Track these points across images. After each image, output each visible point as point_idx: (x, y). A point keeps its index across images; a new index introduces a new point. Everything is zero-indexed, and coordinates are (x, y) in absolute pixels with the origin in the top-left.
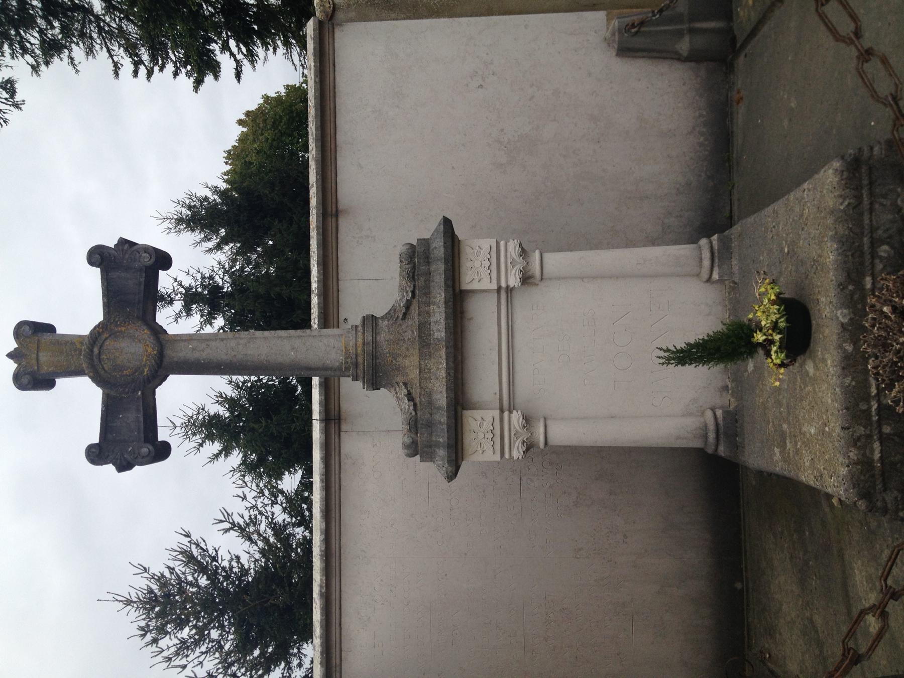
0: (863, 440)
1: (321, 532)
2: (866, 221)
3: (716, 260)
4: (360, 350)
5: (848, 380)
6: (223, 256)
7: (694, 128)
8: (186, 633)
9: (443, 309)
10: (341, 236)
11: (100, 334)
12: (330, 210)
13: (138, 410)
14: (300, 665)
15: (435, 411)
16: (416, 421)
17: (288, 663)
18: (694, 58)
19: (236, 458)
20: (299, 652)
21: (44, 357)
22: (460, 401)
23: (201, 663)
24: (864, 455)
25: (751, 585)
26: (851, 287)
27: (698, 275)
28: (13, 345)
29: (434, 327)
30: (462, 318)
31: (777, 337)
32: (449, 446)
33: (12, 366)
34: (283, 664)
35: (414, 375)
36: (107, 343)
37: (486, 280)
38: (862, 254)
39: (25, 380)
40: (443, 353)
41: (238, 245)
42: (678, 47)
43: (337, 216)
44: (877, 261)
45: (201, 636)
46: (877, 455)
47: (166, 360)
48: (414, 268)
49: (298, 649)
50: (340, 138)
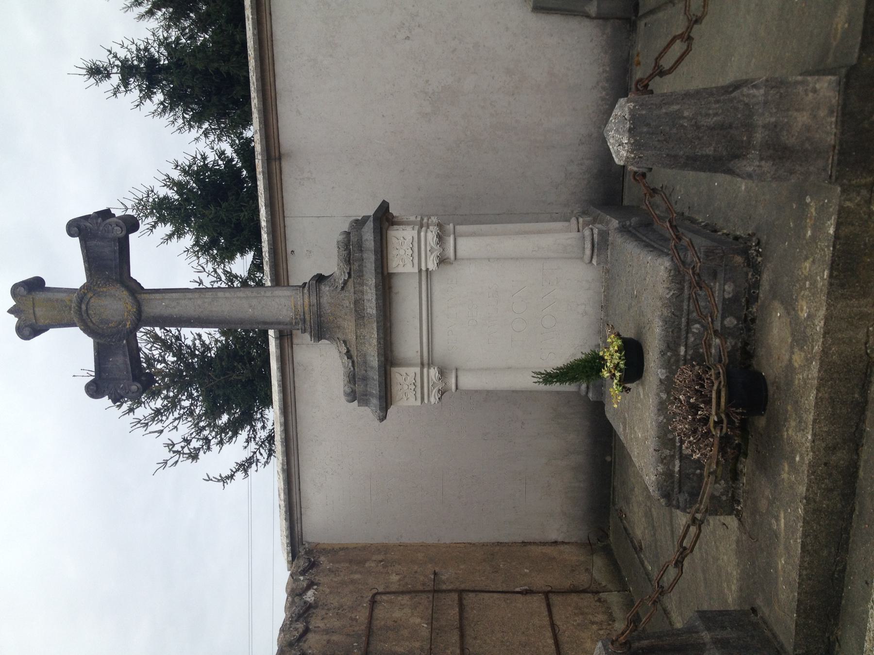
0: (668, 458)
1: (281, 425)
2: (685, 307)
3: (596, 251)
4: (306, 309)
5: (661, 418)
6: (155, 23)
7: (598, 83)
8: (159, 403)
9: (374, 291)
10: (284, 178)
11: (85, 294)
12: (273, 154)
13: (125, 355)
14: (264, 427)
15: (369, 369)
16: (354, 376)
17: (252, 426)
18: (601, 17)
19: (188, 240)
20: (262, 416)
21: (39, 312)
22: (389, 360)
23: (176, 427)
24: (668, 469)
25: (617, 460)
26: (669, 354)
27: (582, 258)
28: (12, 303)
29: (367, 304)
30: (390, 293)
31: (618, 374)
32: (380, 398)
33: (14, 320)
34: (249, 427)
35: (352, 337)
36: (92, 300)
37: (409, 265)
38: (680, 329)
39: (27, 331)
40: (375, 325)
41: (171, 10)
42: (587, 9)
43: (280, 159)
44: (690, 335)
45: (174, 403)
46: (677, 469)
47: (144, 315)
48: (349, 254)
49: (261, 414)
50: (279, 69)
